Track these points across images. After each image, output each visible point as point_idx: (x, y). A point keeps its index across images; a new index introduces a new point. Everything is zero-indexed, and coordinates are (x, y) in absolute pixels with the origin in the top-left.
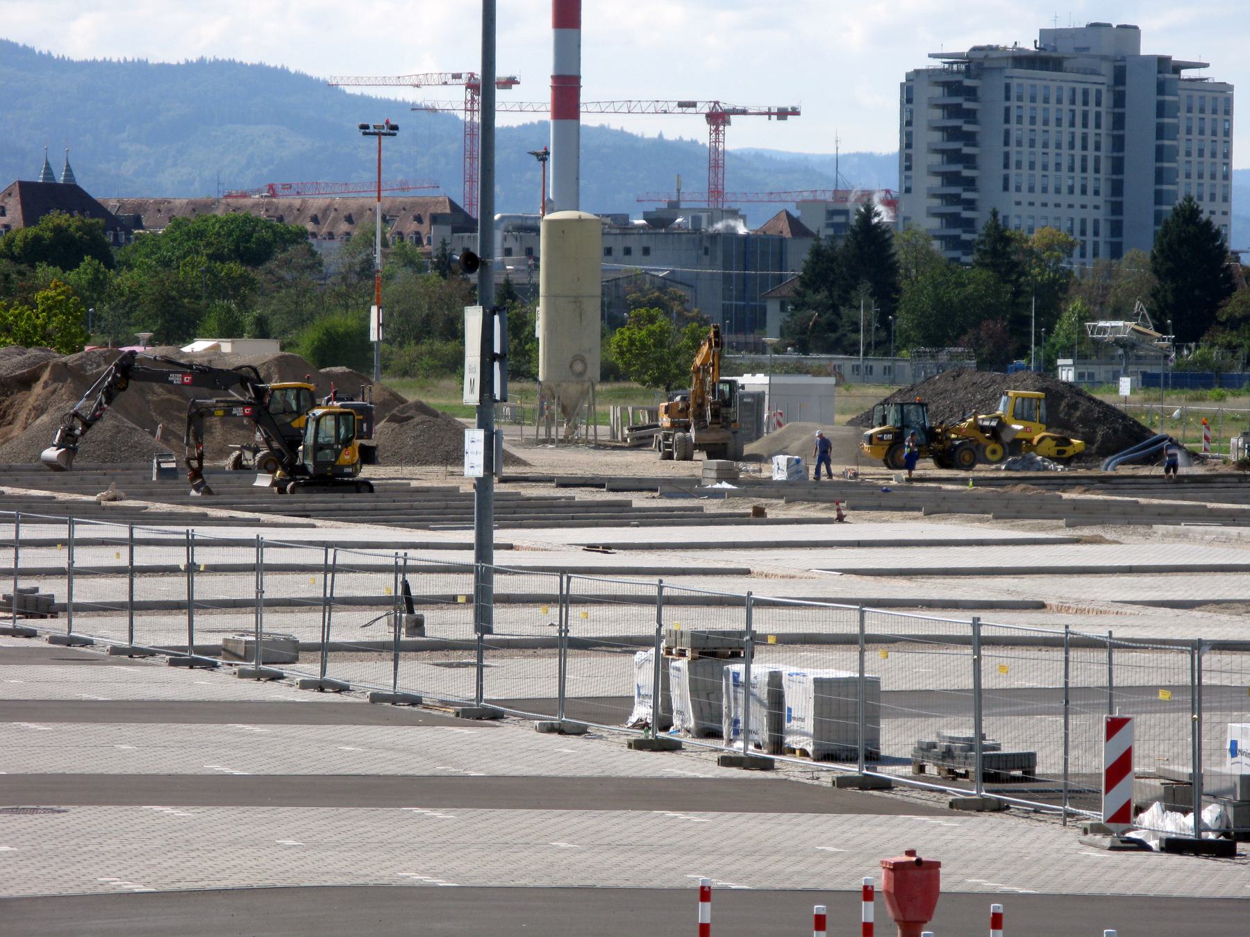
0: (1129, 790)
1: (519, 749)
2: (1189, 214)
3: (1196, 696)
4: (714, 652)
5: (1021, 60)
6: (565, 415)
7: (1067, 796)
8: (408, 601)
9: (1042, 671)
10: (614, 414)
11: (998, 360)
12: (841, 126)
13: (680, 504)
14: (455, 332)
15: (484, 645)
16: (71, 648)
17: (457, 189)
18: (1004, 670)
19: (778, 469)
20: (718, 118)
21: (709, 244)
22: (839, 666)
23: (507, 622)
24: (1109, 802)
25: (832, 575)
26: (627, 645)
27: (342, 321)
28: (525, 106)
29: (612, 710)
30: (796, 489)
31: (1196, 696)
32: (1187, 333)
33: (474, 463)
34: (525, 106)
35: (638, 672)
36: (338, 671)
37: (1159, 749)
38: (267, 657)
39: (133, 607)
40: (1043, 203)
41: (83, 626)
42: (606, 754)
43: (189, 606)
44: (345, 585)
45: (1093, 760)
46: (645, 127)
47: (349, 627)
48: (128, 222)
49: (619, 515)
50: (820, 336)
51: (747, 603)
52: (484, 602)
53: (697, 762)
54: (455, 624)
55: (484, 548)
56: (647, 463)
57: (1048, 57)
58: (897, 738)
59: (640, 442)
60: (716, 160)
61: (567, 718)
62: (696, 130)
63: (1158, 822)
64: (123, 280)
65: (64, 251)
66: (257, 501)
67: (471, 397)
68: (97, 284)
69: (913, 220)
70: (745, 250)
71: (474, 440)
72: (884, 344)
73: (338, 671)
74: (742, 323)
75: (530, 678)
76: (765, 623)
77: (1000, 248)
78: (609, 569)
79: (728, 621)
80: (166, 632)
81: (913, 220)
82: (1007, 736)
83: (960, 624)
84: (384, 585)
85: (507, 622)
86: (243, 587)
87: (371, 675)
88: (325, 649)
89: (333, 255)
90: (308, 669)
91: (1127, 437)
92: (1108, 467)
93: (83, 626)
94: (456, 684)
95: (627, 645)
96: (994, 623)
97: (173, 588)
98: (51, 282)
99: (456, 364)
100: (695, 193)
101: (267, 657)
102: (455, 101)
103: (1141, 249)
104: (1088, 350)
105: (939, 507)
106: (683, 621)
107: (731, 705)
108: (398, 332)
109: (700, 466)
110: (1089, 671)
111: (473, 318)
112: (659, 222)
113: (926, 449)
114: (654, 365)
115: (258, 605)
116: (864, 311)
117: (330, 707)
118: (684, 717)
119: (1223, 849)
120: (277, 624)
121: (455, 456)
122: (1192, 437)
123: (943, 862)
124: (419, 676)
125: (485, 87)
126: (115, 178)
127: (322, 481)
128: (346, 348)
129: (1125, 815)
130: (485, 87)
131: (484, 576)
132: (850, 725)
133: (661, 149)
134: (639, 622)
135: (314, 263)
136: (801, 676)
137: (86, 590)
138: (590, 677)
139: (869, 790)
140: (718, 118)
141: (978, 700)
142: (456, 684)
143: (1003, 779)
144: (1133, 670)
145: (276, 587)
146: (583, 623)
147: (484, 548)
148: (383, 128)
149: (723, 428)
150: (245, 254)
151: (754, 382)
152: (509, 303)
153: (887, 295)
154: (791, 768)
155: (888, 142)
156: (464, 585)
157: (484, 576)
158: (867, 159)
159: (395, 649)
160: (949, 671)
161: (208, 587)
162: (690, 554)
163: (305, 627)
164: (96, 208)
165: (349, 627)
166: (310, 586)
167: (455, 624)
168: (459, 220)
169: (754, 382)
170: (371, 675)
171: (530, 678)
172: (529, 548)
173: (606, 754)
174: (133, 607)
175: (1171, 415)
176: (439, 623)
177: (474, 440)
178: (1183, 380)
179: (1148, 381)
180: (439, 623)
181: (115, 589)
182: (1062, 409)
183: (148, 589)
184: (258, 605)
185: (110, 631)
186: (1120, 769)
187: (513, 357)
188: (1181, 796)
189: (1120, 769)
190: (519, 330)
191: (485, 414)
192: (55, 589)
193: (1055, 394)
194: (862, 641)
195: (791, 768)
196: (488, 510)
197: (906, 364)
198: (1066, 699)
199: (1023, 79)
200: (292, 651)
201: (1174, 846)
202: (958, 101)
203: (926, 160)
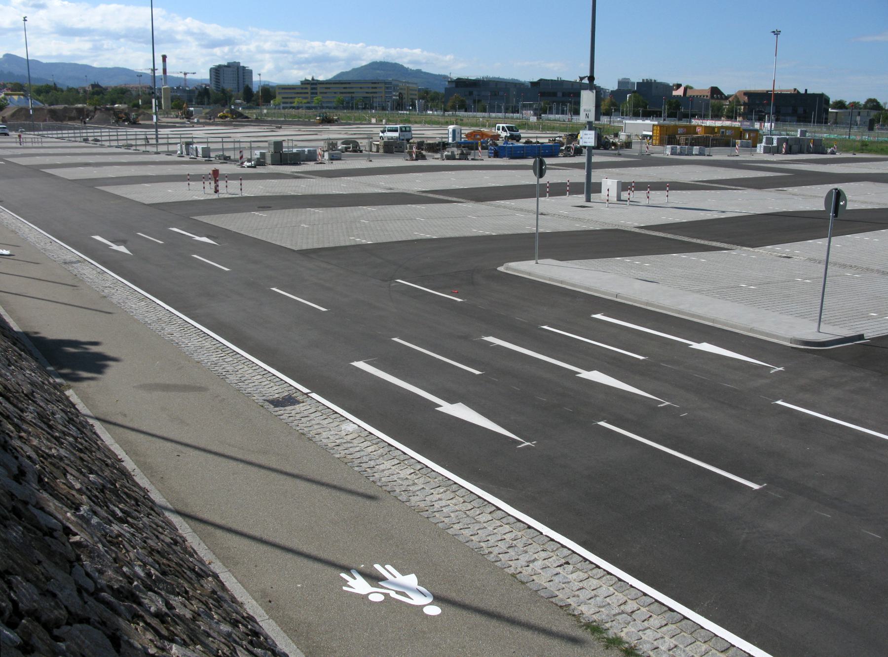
0: (243, 160)
1: (163, 158)
2: (247, 86)
3: (251, 148)
4: (188, 144)
5: (225, 66)
6: (167, 114)
7: (235, 161)
8: (147, 139)
9: (231, 146)
10: (173, 114)
11: (224, 105)
12: (203, 75)
13: (183, 125)
14: (151, 103)
15: (157, 145)
16: (102, 146)
17: (149, 83)
18: (226, 146)
19: (196, 120)
20: (185, 74)
21: (184, 90)
22: (205, 146)
23: (160, 141)
24: (240, 162)
25: (203, 134)
26: (176, 144)
27: (136, 102)
28: (159, 73)
29: (175, 152)
30: (198, 123)
31: (251, 148)
32: (248, 102)
33: (155, 120)
34: (159, 73)
35: (179, 146)
36: (138, 148)
37: (246, 155)
38: (129, 146)
39: (110, 140)
40: (229, 85)
41: (104, 143)
42: (174, 158)
43: (117, 140)
44: (138, 137)
45: (238, 157)
46: (175, 75)
47: (139, 142)
48: (106, 89)
49: (174, 127)
50: (200, 103)
51: (192, 138)
52: (157, 139)
53: (186, 159)
54: (154, 142)
55: (157, 131)
56: (178, 120)
57: (229, 66)
58: (213, 155)
59: (177, 117)
60: (185, 80)
61: (169, 153)
62: (182, 76)
63: (246, 164)
64: (106, 97)
65: (98, 93)
66: (126, 126)
67: (154, 111)
68: (103, 98)
69: (213, 87)
70: (190, 91)
71: (155, 117)
72: (209, 104)
73: (138, 148)
74: (190, 102)
75: (165, 148)
76: (195, 140)
77: (223, 91)
78: (173, 134)
79: (190, 140)
80: (115, 143)
81: (213, 87)
82: (227, 154)
83: (220, 140)
84: (143, 137)
85: (160, 141)
86: (125, 137)
87: (143, 149)
88: (136, 145)
89: (134, 93)
90: (134, 148)
91: (240, 115)
92: (239, 119)
93: (104, 143)
94: (154, 149)
95: (176, 144)
96: (225, 140)
97: (115, 138)
98: (96, 97)
99: (151, 107)
100: (183, 84)
101: (129, 146)
102: (149, 72)
103: (242, 91)
104: (235, 104)
105: (217, 125)
106: (183, 140)
107: (191, 151)
108: (143, 103)
109: (185, 120)
110: (237, 145)
111: (154, 101)
112: (178, 88)
113: (210, 119)
114: (178, 107)
115: (127, 140)
116: (206, 100)
117: (138, 153)
118: (185, 152)
119: (255, 167)
120: (129, 142)
121: (152, 119)
122: (249, 115)
123: (621, 77)
124: (149, 148)
125: (154, 70)
126: (104, 83)
127: (134, 123)
128: (137, 106)
129: (242, 163)
130: (154, 70)
131: (157, 135)
132: (206, 153)
133: (178, 78)
134: (178, 141)
135: (132, 94)
136: (200, 147)
137: (103, 138)
138: (171, 148)
139: (209, 162)
140: (185, 74)
141: (223, 150)
142: (154, 149)
143: (226, 159)
144: (243, 145)
145: (129, 137)
146: (171, 141)
147: (157, 131)
148: (140, 75)
149: (189, 115)
150: (122, 93)
151: (192, 109)
152: (159, 99)
153: (209, 98)
154: (199, 159)
155: (208, 77)
156: (154, 137)
157: (157, 135)
158: (205, 80)
159: (145, 145)
160: (219, 146)
161: (120, 138)
162: (75, 157)
163: (133, 142)
164: (101, 87)
165: (139, 142)
166: (133, 137)
167: (154, 142)
168: (151, 88)
169: (192, 109)
170: (143, 149)
171: (165, 148)
172: (163, 131)
173: (174, 158)
174: (110, 140)
175: (247, 113)
176: (151, 142)
177: (155, 117)
178: (249, 108)
179: (243, 108)
180: (151, 142)
181: (107, 138)
182: (233, 112)
183: (112, 138)
184: (127, 140)
185: (107, 144)
186: (241, 157)
187: (159, 106)
188: (249, 161)
189: (241, 157)
190: (160, 103)
191: (156, 114)
192: (99, 138)
193: (231, 110)
194: (208, 142)
195: (199, 159)
196: (157, 126)
197: (212, 106)
198: (234, 149)
199: (226, 69)
200: (132, 146)
201: (248, 167)
202: (217, 72)
203: (213, 79)
